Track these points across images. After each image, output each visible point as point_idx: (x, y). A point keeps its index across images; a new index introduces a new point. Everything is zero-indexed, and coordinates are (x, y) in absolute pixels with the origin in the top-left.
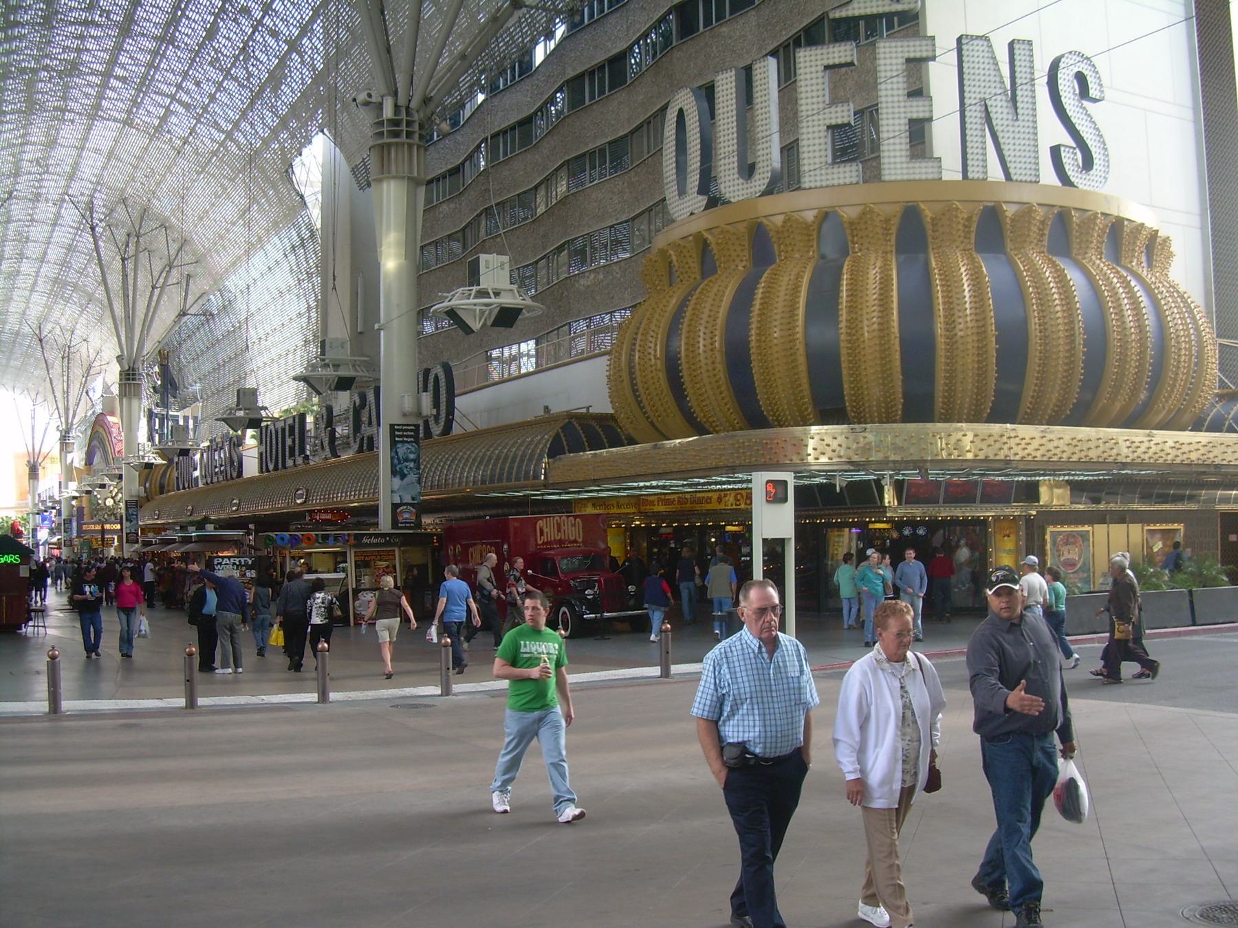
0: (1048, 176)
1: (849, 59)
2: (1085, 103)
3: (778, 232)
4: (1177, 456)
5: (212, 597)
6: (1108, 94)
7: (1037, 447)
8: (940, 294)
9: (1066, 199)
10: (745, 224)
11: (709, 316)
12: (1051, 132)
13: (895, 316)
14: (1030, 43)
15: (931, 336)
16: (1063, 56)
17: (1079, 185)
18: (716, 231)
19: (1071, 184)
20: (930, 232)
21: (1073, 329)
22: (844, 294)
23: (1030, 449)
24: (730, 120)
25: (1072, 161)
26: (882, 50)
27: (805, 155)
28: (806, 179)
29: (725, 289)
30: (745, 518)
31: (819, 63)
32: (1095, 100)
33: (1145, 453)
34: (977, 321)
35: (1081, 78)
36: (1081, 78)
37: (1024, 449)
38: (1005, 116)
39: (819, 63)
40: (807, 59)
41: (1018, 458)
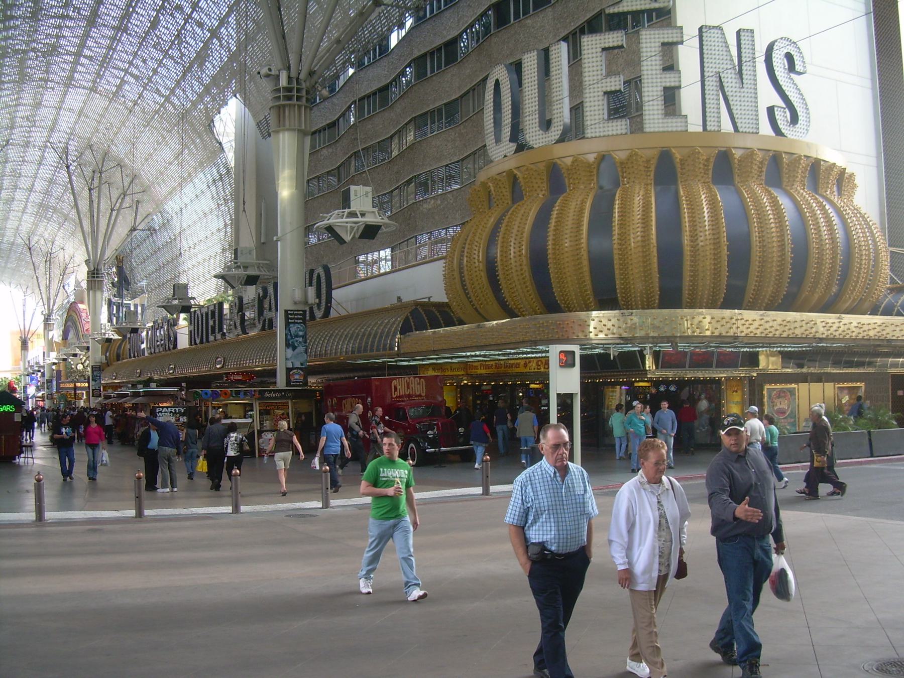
0: (766, 129)
1: (620, 43)
2: (793, 75)
3: (568, 170)
4: (859, 333)
6: (809, 68)
7: (757, 327)
8: (686, 215)
9: (778, 145)
10: (544, 164)
11: (518, 231)
12: (768, 96)
13: (654, 231)
14: (752, 31)
15: (680, 246)
16: (776, 41)
17: (788, 135)
18: (523, 169)
19: (782, 135)
20: (679, 170)
21: (783, 240)
22: (617, 215)
23: (752, 328)
24: (533, 87)
25: (783, 117)
26: (644, 37)
27: (588, 113)
28: (589, 131)
29: (530, 211)
31: (598, 46)
32: (799, 73)
33: (836, 331)
34: (713, 234)
35: (789, 57)
36: (789, 57)
37: (748, 328)
38: (734, 85)
39: (598, 46)
40: (590, 43)
41: (743, 334)
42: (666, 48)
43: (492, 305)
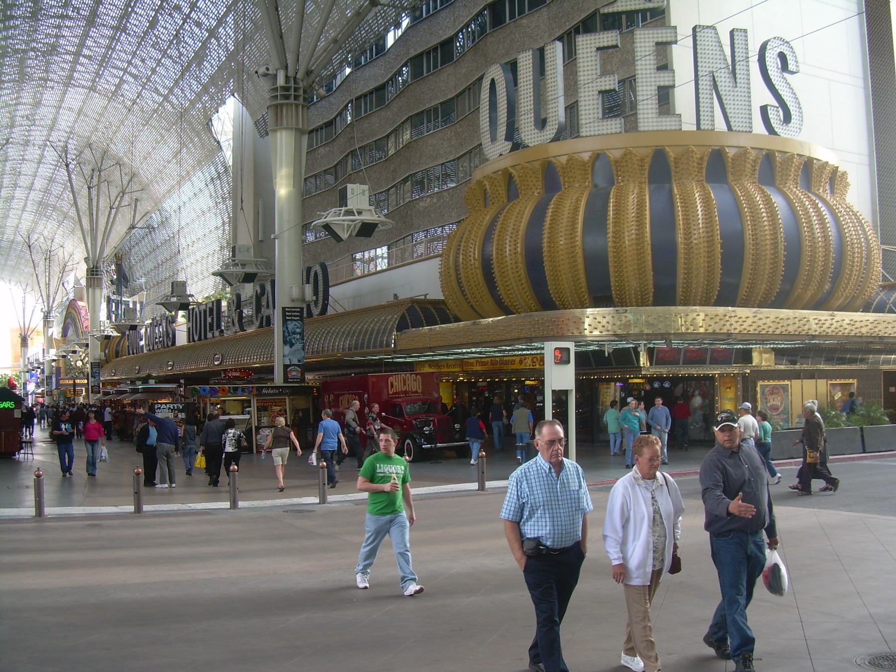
0: (759, 127)
1: (614, 43)
2: (786, 75)
3: (563, 168)
4: (852, 330)
5: (153, 432)
6: (802, 68)
7: (750, 324)
8: (680, 213)
9: (772, 144)
10: (539, 162)
11: (513, 229)
12: (761, 95)
13: (648, 229)
14: (745, 31)
16: (769, 40)
17: (781, 134)
18: (518, 168)
19: (775, 133)
20: (673, 168)
21: (776, 238)
22: (611, 213)
23: (745, 325)
24: (528, 87)
25: (776, 116)
26: (638, 36)
27: (583, 112)
28: (584, 130)
29: (525, 209)
30: (539, 375)
31: (593, 45)
32: (792, 73)
33: (829, 328)
34: (707, 232)
35: (782, 57)
36: (782, 57)
37: (741, 325)
38: (727, 84)
39: (593, 45)
40: (584, 42)
41: (736, 331)
42: (660, 47)
43: (488, 302)
